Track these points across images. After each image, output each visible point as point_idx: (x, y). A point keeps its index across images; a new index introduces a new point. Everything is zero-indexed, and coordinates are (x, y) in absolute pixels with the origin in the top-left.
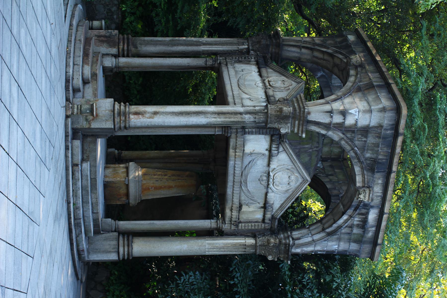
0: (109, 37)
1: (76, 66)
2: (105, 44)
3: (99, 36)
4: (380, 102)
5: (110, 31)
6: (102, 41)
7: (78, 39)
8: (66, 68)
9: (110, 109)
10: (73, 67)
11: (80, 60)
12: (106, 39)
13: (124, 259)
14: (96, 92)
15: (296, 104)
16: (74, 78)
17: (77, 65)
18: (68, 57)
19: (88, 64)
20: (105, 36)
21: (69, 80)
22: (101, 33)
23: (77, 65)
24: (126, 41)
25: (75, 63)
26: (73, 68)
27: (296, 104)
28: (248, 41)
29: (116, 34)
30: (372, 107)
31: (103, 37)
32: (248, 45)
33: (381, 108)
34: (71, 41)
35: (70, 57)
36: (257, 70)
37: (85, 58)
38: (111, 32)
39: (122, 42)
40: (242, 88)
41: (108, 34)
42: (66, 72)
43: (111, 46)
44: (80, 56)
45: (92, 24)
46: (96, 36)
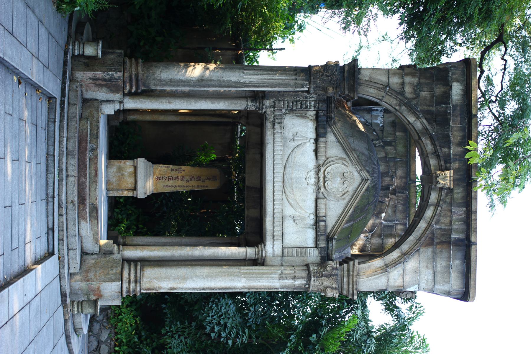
0: (110, 80)
1: (71, 252)
2: (104, 89)
3: (95, 79)
4: (447, 280)
5: (110, 73)
6: (101, 86)
7: (70, 200)
8: (60, 281)
9: (117, 290)
10: (68, 253)
11: (73, 214)
12: (105, 83)
13: (135, 296)
14: (97, 237)
15: (345, 280)
16: (70, 267)
17: (73, 249)
18: (61, 266)
19: (85, 219)
20: (103, 79)
21: (66, 294)
22: (98, 76)
23: (73, 249)
24: (134, 83)
25: (70, 247)
26: (68, 255)
27: (345, 280)
28: (310, 83)
29: (120, 77)
30: (437, 287)
31: (101, 80)
32: (309, 88)
33: (446, 291)
34: (63, 240)
35: (64, 266)
36: (313, 135)
37: (81, 206)
38: (113, 75)
39: (128, 84)
40: (287, 193)
41: (107, 77)
42: (61, 286)
43: (112, 92)
44: (75, 236)
45: (83, 52)
46: (90, 79)
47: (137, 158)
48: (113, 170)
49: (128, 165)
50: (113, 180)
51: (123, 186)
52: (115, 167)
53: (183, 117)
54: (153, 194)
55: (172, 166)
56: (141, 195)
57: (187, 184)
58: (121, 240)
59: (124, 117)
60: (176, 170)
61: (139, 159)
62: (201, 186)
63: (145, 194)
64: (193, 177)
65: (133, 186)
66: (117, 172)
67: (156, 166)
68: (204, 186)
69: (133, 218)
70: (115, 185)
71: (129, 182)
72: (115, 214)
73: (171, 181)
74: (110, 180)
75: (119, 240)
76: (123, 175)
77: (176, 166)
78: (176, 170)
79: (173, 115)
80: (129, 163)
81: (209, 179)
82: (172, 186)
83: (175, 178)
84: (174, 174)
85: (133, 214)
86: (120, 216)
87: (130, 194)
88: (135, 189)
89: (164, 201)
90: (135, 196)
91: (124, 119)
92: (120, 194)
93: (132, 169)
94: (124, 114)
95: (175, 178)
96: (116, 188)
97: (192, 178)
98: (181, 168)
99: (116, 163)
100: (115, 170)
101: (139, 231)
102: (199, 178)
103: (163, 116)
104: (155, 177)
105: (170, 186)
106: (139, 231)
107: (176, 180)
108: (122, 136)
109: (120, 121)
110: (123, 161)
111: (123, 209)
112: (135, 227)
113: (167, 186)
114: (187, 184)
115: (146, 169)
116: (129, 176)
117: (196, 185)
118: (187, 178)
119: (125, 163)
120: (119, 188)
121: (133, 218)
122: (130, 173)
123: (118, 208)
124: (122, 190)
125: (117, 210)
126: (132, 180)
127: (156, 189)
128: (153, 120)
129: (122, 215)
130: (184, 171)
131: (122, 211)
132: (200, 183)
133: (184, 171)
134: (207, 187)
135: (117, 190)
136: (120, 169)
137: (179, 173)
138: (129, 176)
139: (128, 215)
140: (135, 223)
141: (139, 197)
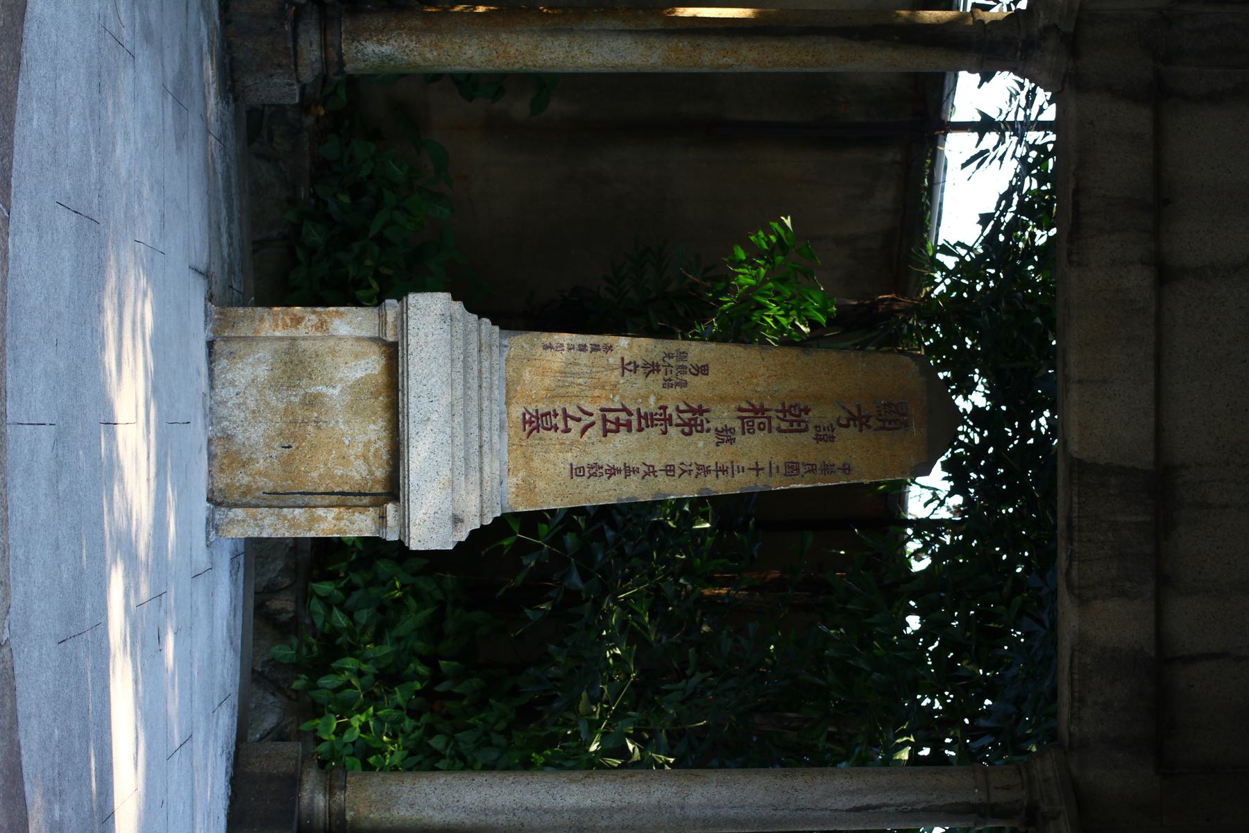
47: (400, 296)
48: (250, 371)
49: (343, 336)
50: (254, 435)
51: (315, 474)
52: (264, 352)
53: (684, 44)
54: (502, 524)
55: (623, 341)
56: (433, 518)
57: (723, 455)
58: (321, 801)
59: (324, 46)
60: (652, 368)
61: (417, 300)
62: (812, 469)
63: (457, 520)
64: (759, 411)
65: (380, 473)
66: (275, 385)
67: (522, 342)
68: (827, 469)
69: (410, 622)
70: (263, 469)
71: (353, 448)
72: (317, 606)
73: (621, 440)
74: (229, 438)
75: (305, 796)
76: (312, 402)
77: (644, 342)
78: (652, 368)
79: (620, 32)
80: (349, 324)
81: (858, 420)
82: (629, 471)
83: (647, 420)
84: (645, 393)
85: (412, 602)
86: (340, 619)
87: (360, 525)
88: (393, 489)
89: (570, 539)
90: (392, 536)
91: (326, 62)
92: (293, 524)
93: (371, 365)
94: (323, 32)
95: (647, 420)
96: (270, 486)
97: (754, 416)
98: (683, 355)
99: (273, 324)
100: (263, 372)
101: (442, 688)
102: (794, 416)
103: (564, 40)
104: (517, 411)
105: (613, 471)
106: (442, 688)
107: (654, 432)
108: (345, 199)
109: (307, 75)
110: (310, 316)
111: (357, 579)
112: (422, 670)
113: (595, 470)
114: (723, 455)
115: (466, 368)
116: (354, 409)
117: (779, 460)
118: (723, 416)
119: (322, 325)
120: (288, 485)
121: (410, 622)
122: (356, 389)
123: (333, 577)
124: (307, 498)
125: (325, 588)
126: (374, 431)
127: (528, 488)
128: (500, 64)
129: (350, 615)
130: (703, 370)
131: (350, 589)
132: (802, 446)
133: (703, 370)
134: (846, 469)
135: (278, 498)
136: (294, 366)
137: (667, 384)
138: (354, 409)
139: (382, 609)
140: (420, 646)
141: (414, 546)
